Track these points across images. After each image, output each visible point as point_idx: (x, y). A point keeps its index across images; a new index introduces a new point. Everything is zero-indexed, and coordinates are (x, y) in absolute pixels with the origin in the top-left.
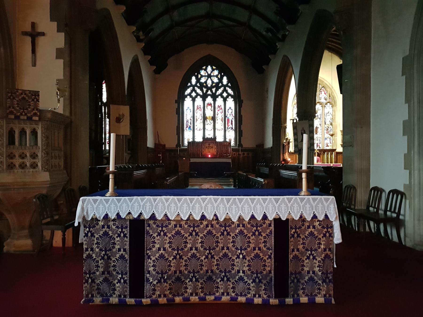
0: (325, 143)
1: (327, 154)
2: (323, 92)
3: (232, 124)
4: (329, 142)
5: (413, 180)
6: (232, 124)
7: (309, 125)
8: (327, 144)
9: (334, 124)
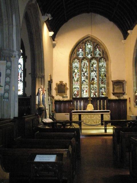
0: (100, 92)
1: (100, 102)
2: (97, 49)
3: (21, 77)
4: (104, 91)
5: (85, 113)
6: (21, 77)
7: (6, 66)
8: (102, 93)
9: (107, 75)
